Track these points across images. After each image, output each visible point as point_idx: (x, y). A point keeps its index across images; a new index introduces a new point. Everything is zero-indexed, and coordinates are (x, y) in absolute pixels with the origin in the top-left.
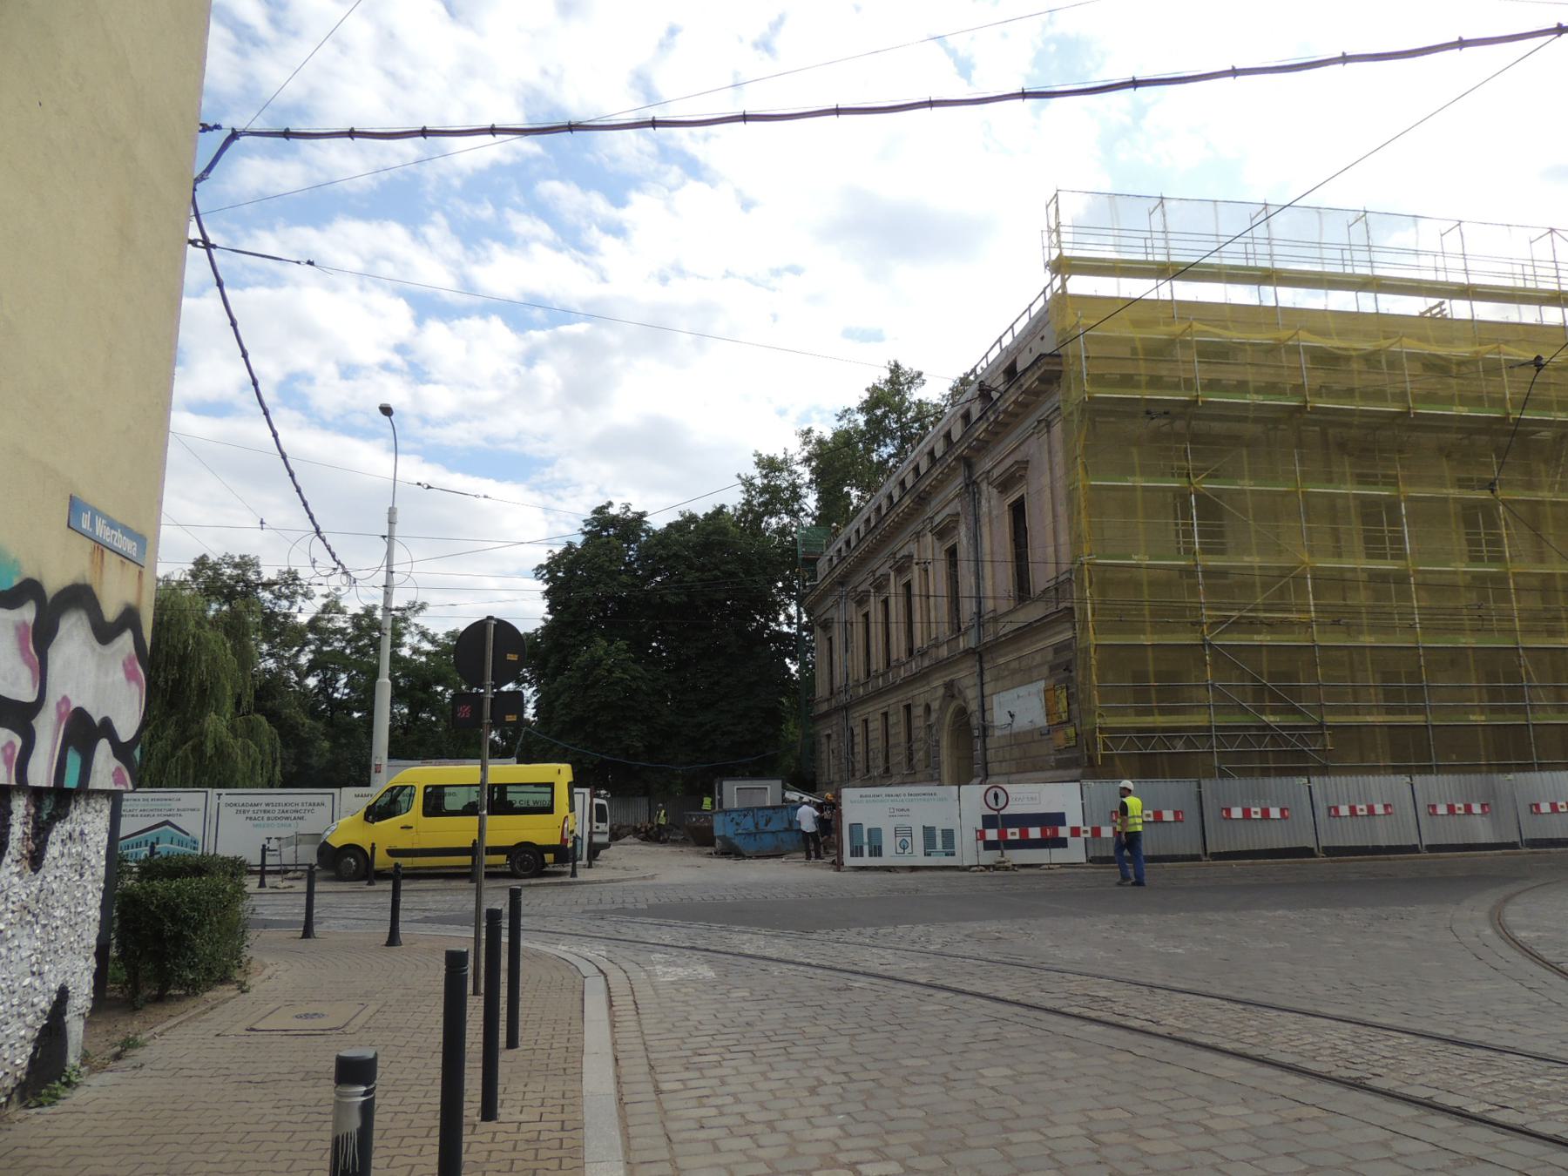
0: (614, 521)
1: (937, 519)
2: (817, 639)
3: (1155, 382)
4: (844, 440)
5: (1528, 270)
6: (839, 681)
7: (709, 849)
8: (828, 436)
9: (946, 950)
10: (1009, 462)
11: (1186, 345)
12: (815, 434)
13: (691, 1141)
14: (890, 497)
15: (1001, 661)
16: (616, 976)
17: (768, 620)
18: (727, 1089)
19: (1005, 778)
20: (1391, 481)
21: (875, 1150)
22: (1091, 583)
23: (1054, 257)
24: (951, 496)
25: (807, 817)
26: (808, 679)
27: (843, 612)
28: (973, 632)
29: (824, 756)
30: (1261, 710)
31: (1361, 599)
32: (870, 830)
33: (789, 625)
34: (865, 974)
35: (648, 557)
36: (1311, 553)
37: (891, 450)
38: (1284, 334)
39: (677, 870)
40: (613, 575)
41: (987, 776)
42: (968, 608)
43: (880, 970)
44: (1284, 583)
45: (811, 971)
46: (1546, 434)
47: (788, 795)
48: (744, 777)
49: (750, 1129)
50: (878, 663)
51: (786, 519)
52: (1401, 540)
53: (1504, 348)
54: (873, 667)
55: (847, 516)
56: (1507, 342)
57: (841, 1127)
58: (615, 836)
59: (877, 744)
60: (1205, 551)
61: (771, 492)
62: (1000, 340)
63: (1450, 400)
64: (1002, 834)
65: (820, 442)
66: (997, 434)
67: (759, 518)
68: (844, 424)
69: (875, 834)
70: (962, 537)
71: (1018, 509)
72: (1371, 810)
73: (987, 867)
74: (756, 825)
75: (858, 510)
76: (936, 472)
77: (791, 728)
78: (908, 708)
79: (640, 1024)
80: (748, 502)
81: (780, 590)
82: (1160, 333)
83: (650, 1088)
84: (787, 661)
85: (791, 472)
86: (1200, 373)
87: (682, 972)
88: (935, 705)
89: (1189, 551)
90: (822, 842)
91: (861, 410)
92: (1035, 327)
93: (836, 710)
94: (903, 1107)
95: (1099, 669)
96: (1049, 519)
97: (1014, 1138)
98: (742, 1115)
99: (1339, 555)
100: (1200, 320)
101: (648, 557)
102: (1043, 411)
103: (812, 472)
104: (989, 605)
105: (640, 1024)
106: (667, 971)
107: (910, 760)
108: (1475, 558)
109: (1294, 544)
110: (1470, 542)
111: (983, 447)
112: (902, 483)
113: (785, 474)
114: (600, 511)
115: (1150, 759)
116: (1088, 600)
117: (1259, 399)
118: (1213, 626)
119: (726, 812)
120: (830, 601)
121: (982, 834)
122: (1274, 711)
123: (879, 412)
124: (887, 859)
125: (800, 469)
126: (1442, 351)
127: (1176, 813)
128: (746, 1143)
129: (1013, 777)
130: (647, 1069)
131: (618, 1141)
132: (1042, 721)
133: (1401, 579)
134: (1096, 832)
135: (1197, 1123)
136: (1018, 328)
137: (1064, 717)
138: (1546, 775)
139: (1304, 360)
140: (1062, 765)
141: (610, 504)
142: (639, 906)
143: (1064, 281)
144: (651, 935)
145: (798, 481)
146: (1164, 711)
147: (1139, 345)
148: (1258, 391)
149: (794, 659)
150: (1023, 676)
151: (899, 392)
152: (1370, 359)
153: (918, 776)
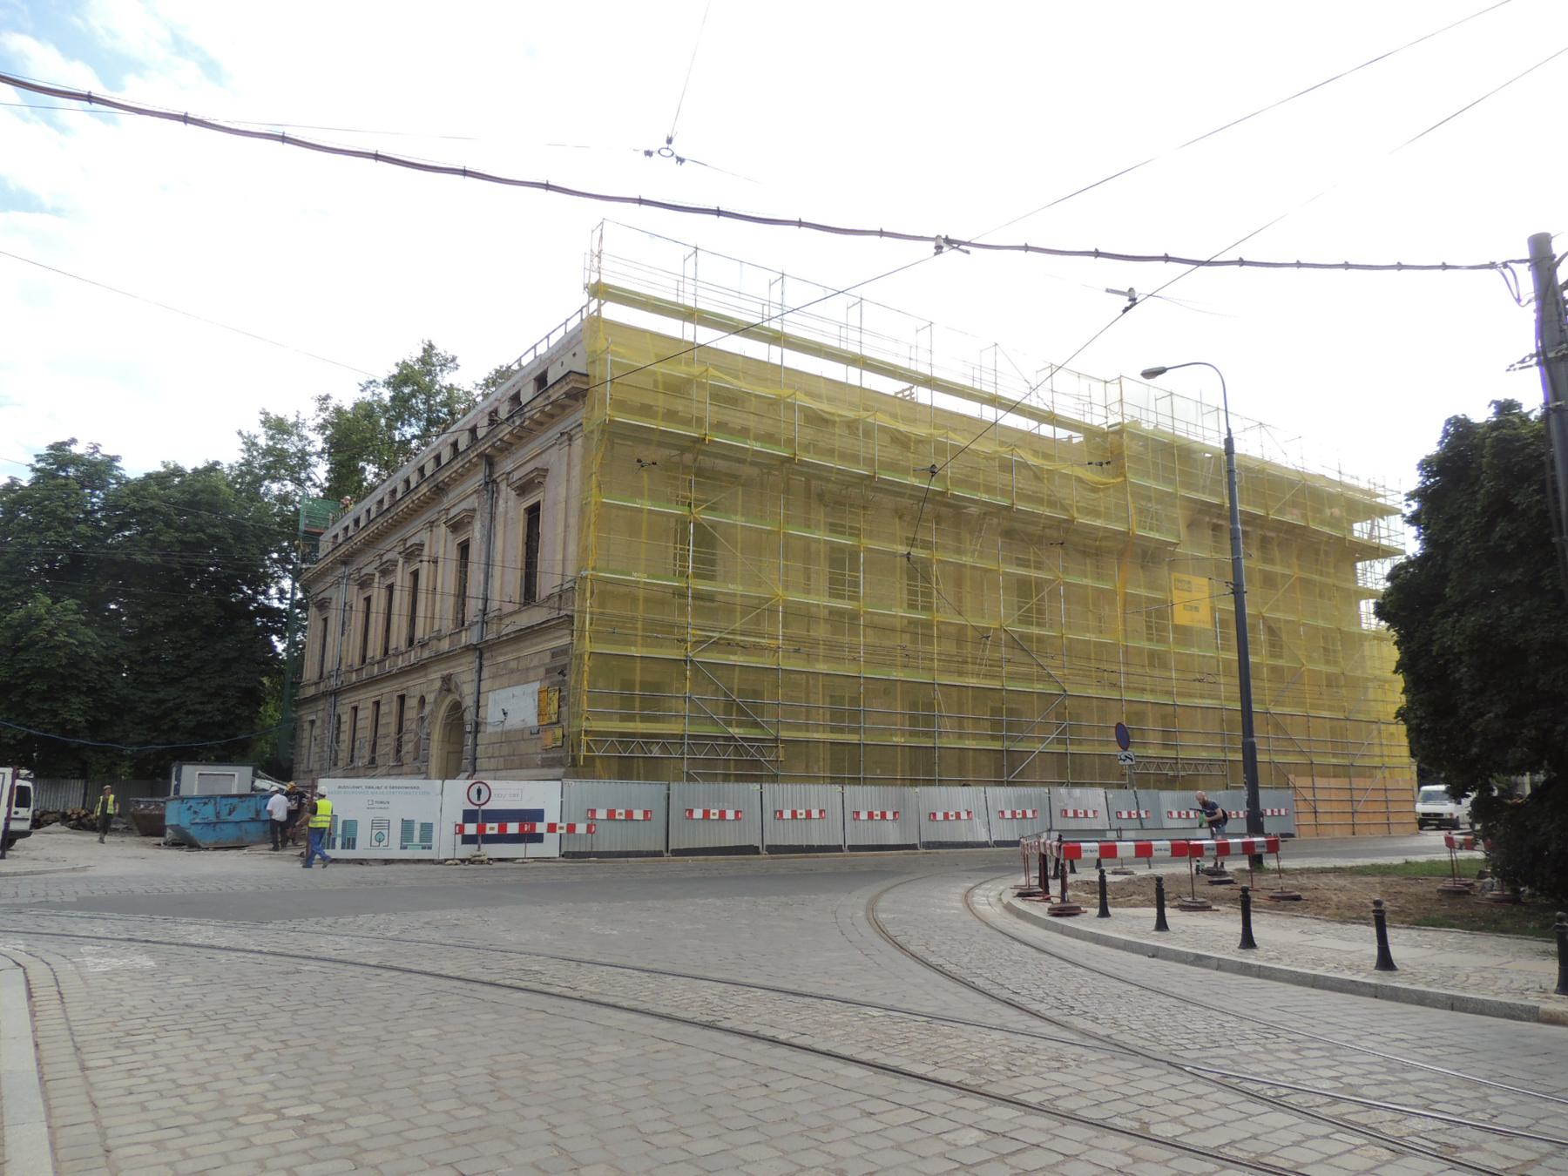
0: (77, 460)
1: (453, 512)
2: (312, 618)
3: (671, 416)
4: (366, 411)
5: (977, 374)
6: (330, 665)
7: (160, 840)
8: (348, 406)
9: (402, 936)
10: (529, 467)
11: (701, 386)
12: (332, 404)
13: (117, 1105)
14: (407, 482)
15: (501, 659)
16: (38, 972)
17: (256, 593)
18: (161, 1061)
19: (492, 774)
20: (855, 532)
21: (300, 1097)
22: (592, 593)
23: (593, 281)
24: (469, 491)
25: (279, 806)
26: (297, 662)
27: (343, 595)
28: (477, 628)
29: (305, 743)
30: (729, 723)
31: (821, 632)
32: (345, 822)
33: (280, 600)
34: (317, 959)
35: (117, 507)
36: (786, 588)
37: (415, 430)
38: (785, 392)
39: (122, 861)
40: (67, 523)
41: (475, 771)
42: (473, 606)
43: (333, 955)
44: (761, 610)
45: (260, 958)
46: (974, 510)
47: (260, 784)
48: (208, 762)
49: (180, 1091)
50: (375, 650)
51: (290, 487)
52: (857, 584)
53: (951, 434)
54: (370, 654)
55: (360, 493)
56: (954, 430)
57: (272, 1083)
58: (37, 823)
59: (365, 733)
60: (697, 576)
61: (280, 460)
62: (534, 347)
63: (905, 471)
64: (481, 829)
65: (339, 411)
66: (521, 438)
67: (258, 480)
68: (368, 396)
69: (350, 826)
70: (476, 533)
71: (533, 513)
72: (809, 814)
73: (463, 861)
74: (218, 814)
75: (372, 488)
76: (457, 465)
77: (271, 710)
78: (402, 698)
79: (64, 1011)
80: (248, 463)
81: (275, 561)
82: (679, 371)
83: (76, 1066)
84: (274, 638)
85: (301, 438)
86: (710, 413)
87: (117, 963)
88: (430, 698)
89: (683, 574)
90: (294, 833)
91: (388, 384)
92: (569, 342)
93: (325, 695)
94: (333, 1064)
95: (591, 674)
96: (561, 529)
97: (426, 1080)
98: (174, 1081)
99: (808, 592)
100: (717, 368)
101: (117, 507)
102: (565, 425)
103: (325, 441)
104: (494, 605)
105: (64, 1011)
106: (96, 963)
107: (398, 751)
108: (912, 606)
109: (772, 576)
110: (910, 592)
111: (506, 448)
112: (421, 470)
113: (295, 438)
114: (59, 447)
115: (629, 760)
116: (586, 608)
117: (757, 447)
118: (697, 643)
119: (183, 799)
120: (330, 579)
121: (461, 829)
122: (740, 724)
123: (407, 390)
124: (362, 850)
125: (312, 436)
126: (903, 428)
127: (646, 813)
128: (176, 1102)
129: (499, 774)
130: (72, 1050)
131: (41, 1107)
132: (533, 721)
133: (854, 616)
134: (571, 828)
135: (580, 1059)
136: (554, 339)
137: (554, 719)
138: (943, 789)
139: (798, 417)
140: (548, 763)
141: (73, 441)
142: (66, 899)
143: (600, 305)
144: (82, 928)
145: (309, 449)
146: (645, 719)
147: (660, 378)
148: (758, 438)
149: (282, 638)
150: (520, 675)
151: (429, 373)
152: (851, 425)
153: (405, 768)
